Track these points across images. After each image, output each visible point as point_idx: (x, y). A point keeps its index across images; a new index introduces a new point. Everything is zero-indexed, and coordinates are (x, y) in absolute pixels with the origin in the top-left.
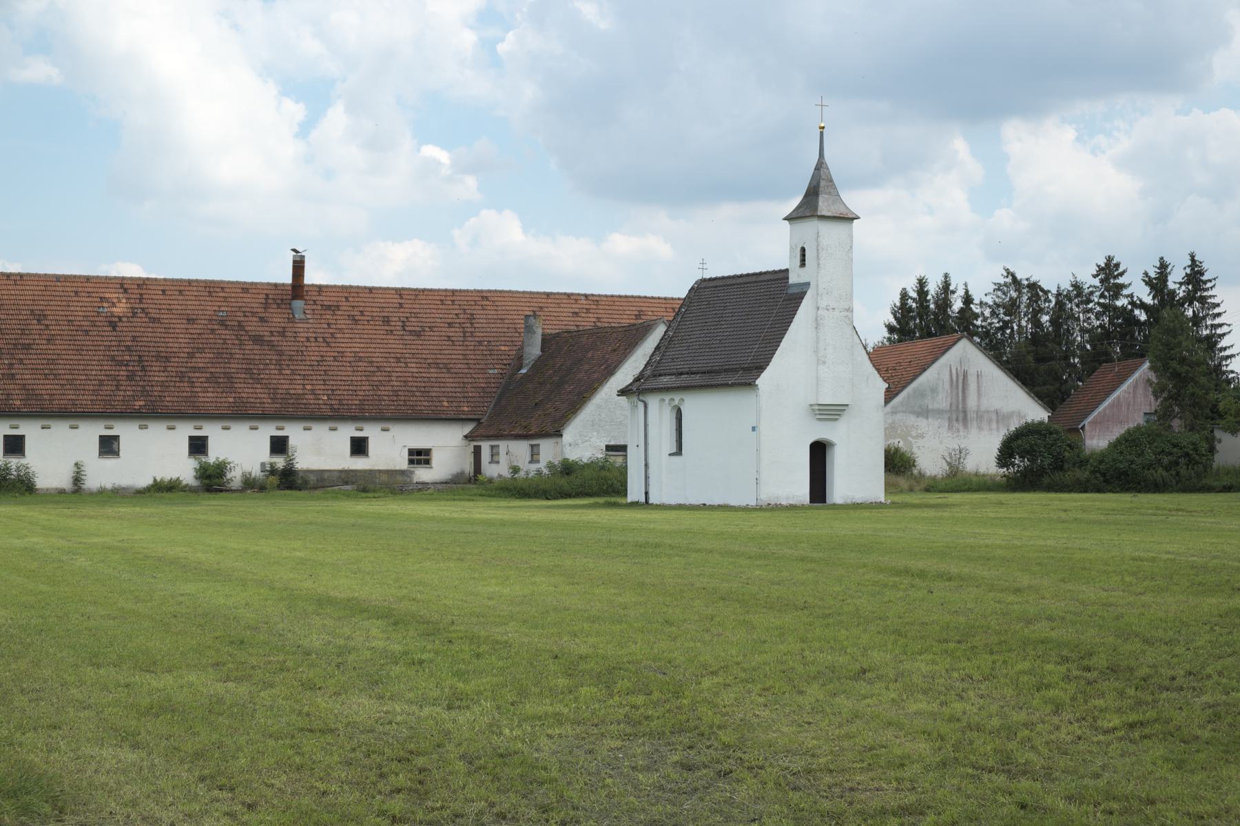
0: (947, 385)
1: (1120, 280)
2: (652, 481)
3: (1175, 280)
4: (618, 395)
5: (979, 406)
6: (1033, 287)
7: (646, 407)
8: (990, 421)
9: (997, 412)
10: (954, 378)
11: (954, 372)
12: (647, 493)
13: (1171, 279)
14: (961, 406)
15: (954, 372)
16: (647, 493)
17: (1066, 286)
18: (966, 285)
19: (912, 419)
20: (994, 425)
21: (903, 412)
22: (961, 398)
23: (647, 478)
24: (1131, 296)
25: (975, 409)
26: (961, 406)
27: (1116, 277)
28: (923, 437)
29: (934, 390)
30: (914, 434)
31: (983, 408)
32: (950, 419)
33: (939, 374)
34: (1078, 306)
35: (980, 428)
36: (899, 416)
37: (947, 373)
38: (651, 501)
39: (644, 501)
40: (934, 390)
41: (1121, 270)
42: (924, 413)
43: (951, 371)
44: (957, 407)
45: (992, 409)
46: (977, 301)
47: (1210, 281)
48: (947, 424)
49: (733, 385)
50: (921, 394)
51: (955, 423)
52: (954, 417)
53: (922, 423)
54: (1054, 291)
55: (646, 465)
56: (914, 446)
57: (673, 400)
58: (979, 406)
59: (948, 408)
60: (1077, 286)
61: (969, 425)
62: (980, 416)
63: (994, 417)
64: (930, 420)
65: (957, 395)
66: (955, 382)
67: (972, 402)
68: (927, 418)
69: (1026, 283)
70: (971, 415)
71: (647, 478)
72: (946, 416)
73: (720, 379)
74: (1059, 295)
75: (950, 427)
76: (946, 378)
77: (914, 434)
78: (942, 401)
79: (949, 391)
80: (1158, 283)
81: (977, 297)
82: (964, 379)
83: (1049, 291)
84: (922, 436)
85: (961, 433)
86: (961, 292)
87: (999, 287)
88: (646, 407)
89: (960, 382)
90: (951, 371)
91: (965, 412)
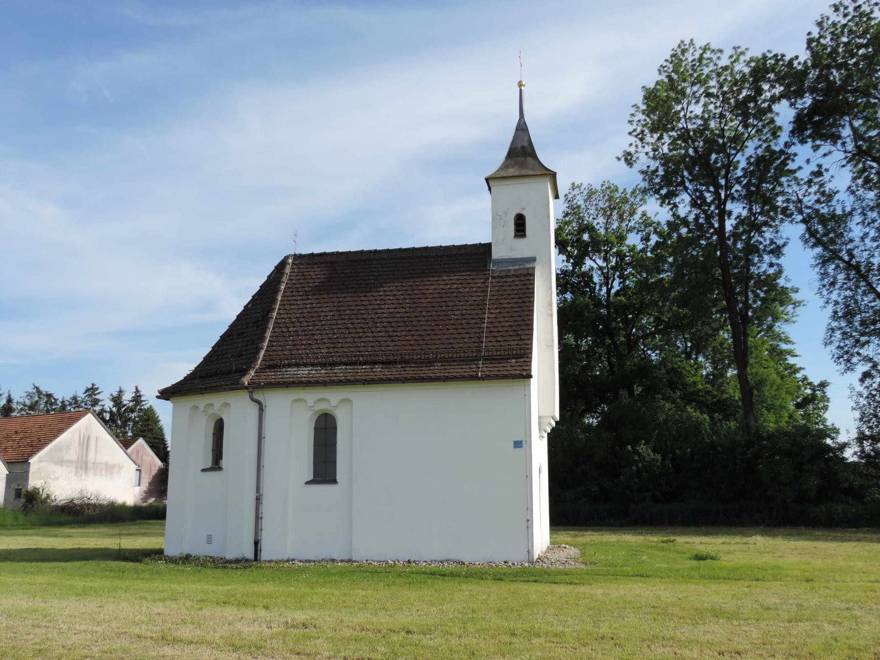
0: (77, 443)
1: (97, 397)
2: (265, 524)
3: (127, 398)
4: (158, 397)
5: (95, 459)
6: (49, 396)
7: (261, 410)
8: (101, 470)
9: (106, 464)
10: (82, 440)
11: (82, 435)
12: (257, 543)
13: (124, 398)
14: (84, 459)
15: (82, 435)
16: (257, 543)
17: (68, 397)
18: (9, 391)
19: (52, 467)
20: (104, 473)
21: (46, 461)
22: (85, 453)
23: (258, 518)
24: (103, 406)
25: (93, 461)
26: (84, 459)
27: (95, 395)
28: (58, 480)
29: (68, 447)
30: (52, 477)
31: (98, 461)
32: (76, 467)
33: (72, 436)
34: (74, 408)
35: (95, 474)
36: (43, 464)
37: (78, 436)
38: (265, 555)
39: (250, 555)
40: (68, 447)
41: (99, 391)
42: (60, 462)
43: (80, 435)
44: (82, 459)
45: (103, 462)
46: (15, 401)
47: (145, 401)
48: (74, 471)
49: (431, 380)
50: (58, 449)
51: (79, 470)
52: (79, 466)
53: (59, 470)
54: (61, 400)
55: (258, 500)
56: (52, 485)
57: (211, 405)
58: (95, 459)
59: (76, 460)
60: (75, 398)
61: (89, 471)
62: (96, 466)
63: (104, 467)
64: (64, 467)
65: (83, 451)
66: (82, 442)
67: (91, 456)
68: (62, 466)
69: (45, 393)
70: (90, 465)
71: (258, 518)
72: (74, 465)
73: (437, 369)
74: (63, 402)
75: (76, 473)
76: (77, 438)
77: (52, 477)
78: (72, 455)
79: (78, 448)
80: (117, 400)
81: (16, 398)
82: (87, 441)
83: (58, 399)
84: (57, 479)
85: (83, 478)
86: (6, 395)
87: (30, 395)
88: (261, 410)
89: (85, 442)
90: (80, 435)
91: (86, 463)
